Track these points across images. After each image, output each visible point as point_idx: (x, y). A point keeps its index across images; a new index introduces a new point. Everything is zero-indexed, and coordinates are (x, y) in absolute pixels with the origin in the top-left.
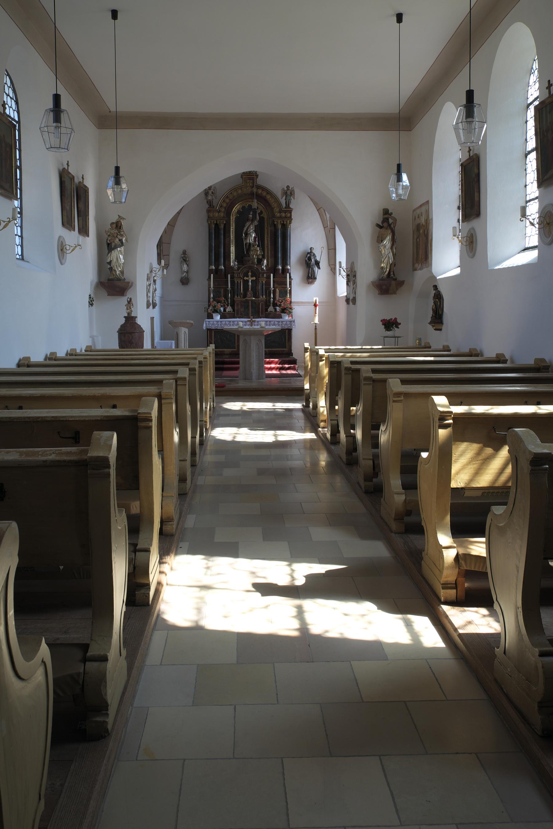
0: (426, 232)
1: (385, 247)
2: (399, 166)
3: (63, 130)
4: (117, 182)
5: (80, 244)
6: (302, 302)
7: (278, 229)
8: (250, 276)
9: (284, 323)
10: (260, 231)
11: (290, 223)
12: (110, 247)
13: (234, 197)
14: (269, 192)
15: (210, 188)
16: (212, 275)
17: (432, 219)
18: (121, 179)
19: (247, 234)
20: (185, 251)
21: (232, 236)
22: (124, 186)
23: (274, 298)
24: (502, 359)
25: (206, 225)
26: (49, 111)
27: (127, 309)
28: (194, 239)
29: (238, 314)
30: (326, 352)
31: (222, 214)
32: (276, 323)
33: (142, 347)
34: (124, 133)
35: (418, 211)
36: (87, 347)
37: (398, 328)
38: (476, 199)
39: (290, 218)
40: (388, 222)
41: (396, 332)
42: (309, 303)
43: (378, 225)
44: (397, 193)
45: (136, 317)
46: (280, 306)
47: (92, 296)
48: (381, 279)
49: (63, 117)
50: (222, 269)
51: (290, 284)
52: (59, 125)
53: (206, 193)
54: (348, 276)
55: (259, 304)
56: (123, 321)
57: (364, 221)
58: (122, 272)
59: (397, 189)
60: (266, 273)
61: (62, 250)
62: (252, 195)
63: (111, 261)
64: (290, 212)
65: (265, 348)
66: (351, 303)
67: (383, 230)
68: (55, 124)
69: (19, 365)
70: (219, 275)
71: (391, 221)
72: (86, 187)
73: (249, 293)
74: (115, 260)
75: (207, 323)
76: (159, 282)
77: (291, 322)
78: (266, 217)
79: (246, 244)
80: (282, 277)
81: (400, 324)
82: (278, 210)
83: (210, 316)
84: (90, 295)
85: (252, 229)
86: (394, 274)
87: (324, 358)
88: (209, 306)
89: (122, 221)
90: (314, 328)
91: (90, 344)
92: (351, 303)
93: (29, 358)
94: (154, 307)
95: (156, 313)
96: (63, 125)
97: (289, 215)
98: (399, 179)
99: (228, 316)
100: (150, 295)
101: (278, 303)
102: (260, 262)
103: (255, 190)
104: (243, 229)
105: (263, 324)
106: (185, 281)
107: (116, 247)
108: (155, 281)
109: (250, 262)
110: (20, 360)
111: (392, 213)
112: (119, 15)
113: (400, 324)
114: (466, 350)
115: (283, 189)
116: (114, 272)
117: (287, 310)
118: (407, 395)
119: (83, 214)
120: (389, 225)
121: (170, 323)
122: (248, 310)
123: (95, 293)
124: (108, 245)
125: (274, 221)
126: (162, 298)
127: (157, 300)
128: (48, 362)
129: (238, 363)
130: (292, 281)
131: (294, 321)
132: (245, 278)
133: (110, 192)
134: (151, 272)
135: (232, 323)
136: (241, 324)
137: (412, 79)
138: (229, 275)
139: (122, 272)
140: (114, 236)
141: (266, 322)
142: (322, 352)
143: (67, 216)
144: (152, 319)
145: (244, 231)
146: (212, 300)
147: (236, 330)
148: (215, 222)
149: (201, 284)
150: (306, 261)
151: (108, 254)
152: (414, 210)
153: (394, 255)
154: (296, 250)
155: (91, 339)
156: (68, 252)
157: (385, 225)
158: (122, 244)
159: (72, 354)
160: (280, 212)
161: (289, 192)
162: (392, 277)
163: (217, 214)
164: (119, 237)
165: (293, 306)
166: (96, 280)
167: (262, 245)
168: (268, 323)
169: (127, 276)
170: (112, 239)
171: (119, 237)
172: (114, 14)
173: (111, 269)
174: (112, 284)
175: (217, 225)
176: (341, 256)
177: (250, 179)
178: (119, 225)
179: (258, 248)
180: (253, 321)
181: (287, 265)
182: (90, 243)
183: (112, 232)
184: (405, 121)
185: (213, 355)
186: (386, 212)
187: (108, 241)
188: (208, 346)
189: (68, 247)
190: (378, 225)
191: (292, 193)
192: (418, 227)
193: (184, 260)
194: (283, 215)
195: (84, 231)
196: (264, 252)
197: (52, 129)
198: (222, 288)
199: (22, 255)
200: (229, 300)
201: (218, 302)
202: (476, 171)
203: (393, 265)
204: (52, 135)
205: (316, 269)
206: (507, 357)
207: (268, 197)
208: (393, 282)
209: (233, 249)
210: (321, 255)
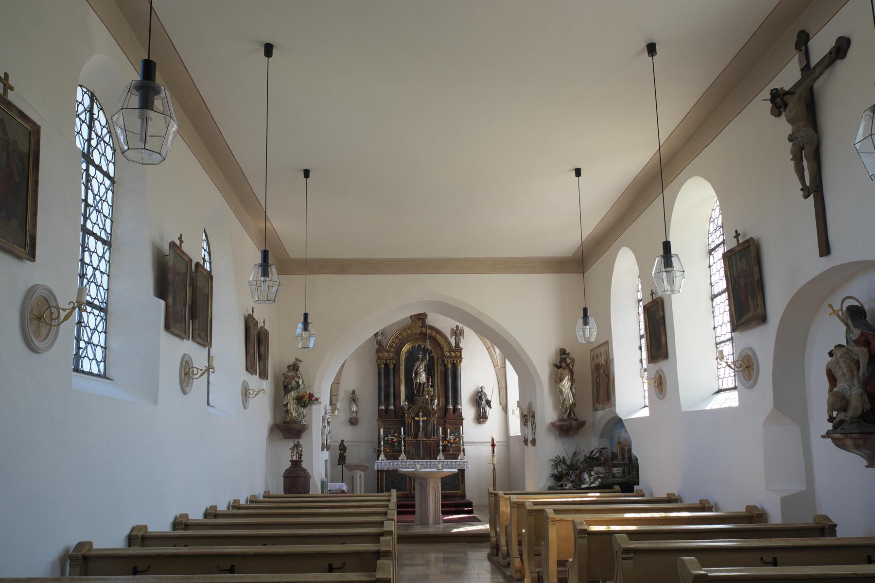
2: (585, 310)
10: (430, 371)
14: (438, 332)
17: (613, 359)
19: (416, 374)
21: (402, 377)
24: (707, 505)
35: (597, 351)
38: (663, 341)
39: (460, 358)
53: (376, 335)
56: (289, 465)
59: (584, 332)
65: (442, 490)
66: (529, 444)
68: (262, 278)
69: (206, 515)
71: (568, 361)
78: (435, 357)
85: (422, 369)
92: (529, 444)
100: (325, 437)
103: (424, 330)
105: (418, 466)
106: (353, 422)
110: (207, 510)
112: (311, 174)
114: (663, 495)
118: (637, 551)
119: (263, 357)
120: (568, 365)
124: (285, 387)
125: (443, 361)
128: (232, 511)
129: (414, 506)
132: (417, 418)
137: (590, 226)
145: (415, 368)
152: (592, 350)
154: (467, 390)
157: (564, 364)
159: (253, 500)
161: (458, 332)
172: (307, 173)
173: (287, 411)
174: (288, 428)
175: (386, 365)
177: (419, 319)
182: (266, 385)
184: (581, 264)
186: (563, 352)
189: (251, 392)
191: (462, 333)
195: (263, 375)
202: (661, 313)
205: (487, 408)
207: (438, 337)
208: (574, 423)
209: (403, 389)
210: (492, 394)
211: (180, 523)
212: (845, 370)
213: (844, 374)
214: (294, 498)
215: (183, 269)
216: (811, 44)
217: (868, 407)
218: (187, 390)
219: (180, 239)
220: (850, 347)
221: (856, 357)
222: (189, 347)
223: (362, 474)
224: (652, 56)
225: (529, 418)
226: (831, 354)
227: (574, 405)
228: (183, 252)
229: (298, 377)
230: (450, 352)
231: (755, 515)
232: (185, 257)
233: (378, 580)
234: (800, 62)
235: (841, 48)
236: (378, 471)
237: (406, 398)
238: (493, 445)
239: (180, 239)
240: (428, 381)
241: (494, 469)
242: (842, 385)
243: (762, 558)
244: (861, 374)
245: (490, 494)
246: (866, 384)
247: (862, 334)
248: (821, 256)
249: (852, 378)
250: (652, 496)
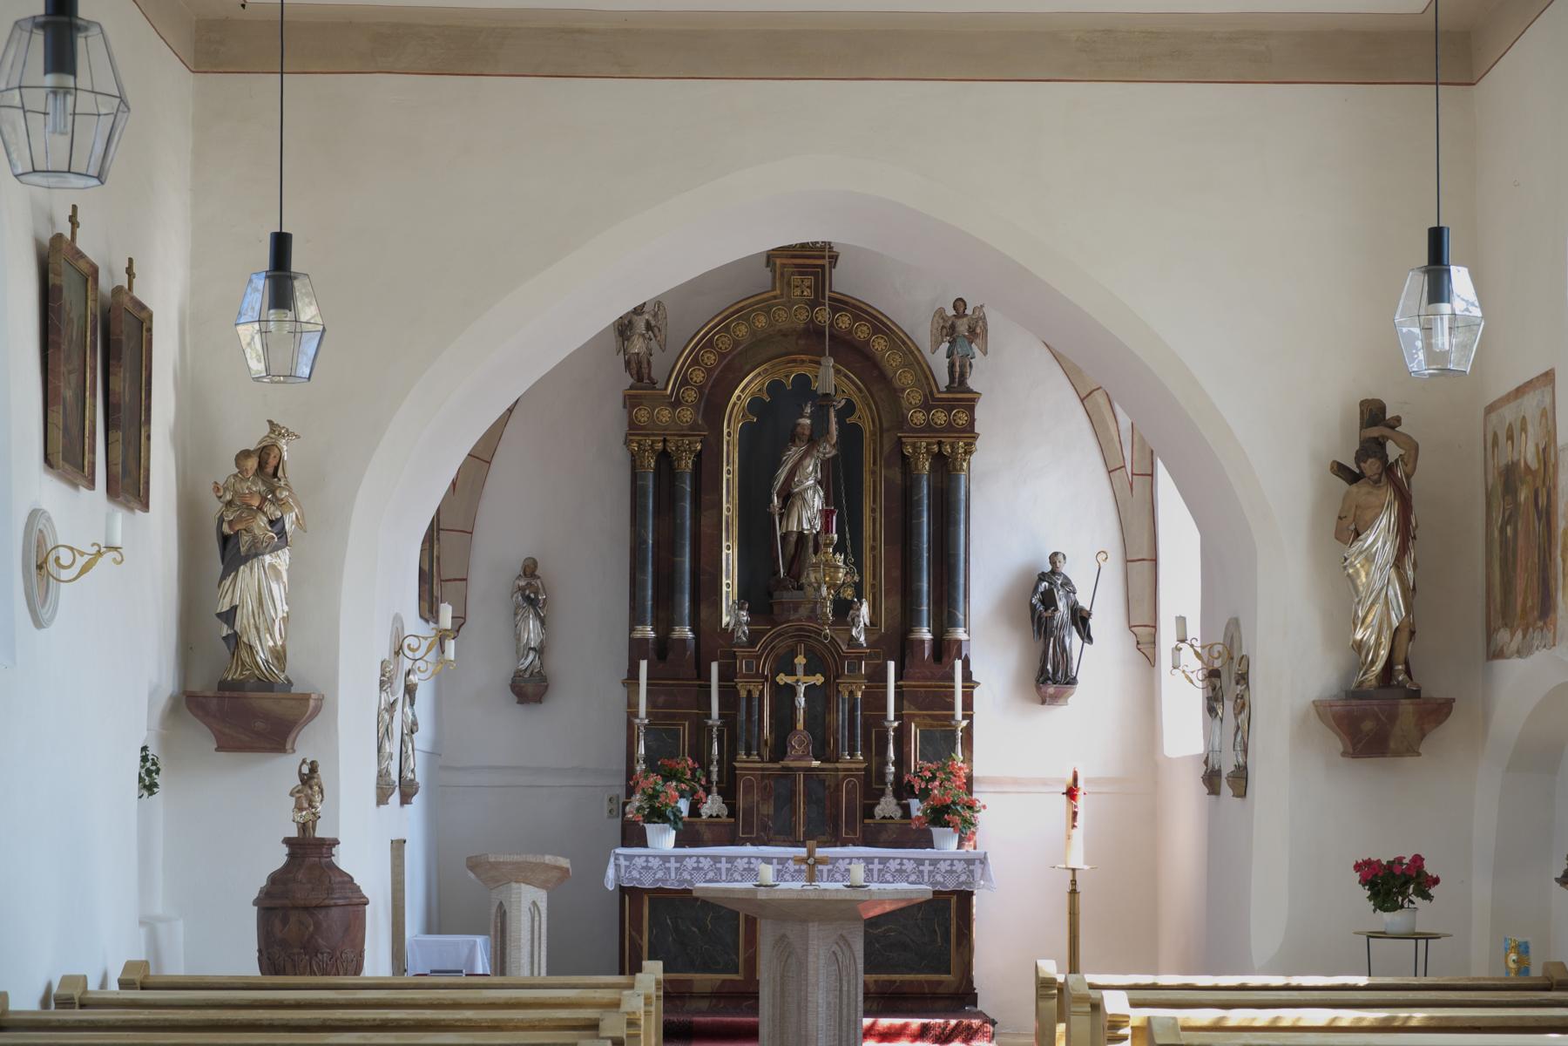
0: (1542, 501)
1: (1370, 559)
2: (1437, 238)
3: (85, 102)
4: (281, 294)
5: (118, 542)
6: (1016, 781)
7: (919, 477)
8: (800, 670)
9: (944, 866)
11: (968, 452)
12: (235, 552)
13: (736, 344)
14: (880, 325)
15: (638, 311)
16: (644, 665)
18: (296, 283)
19: (788, 497)
20: (535, 563)
21: (729, 506)
22: (307, 310)
23: (901, 762)
25: (621, 456)
26: (29, 26)
27: (300, 808)
28: (574, 520)
29: (748, 826)
30: (1135, 1004)
31: (687, 415)
32: (909, 866)
33: (358, 969)
34: (308, 91)
35: (1509, 414)
36: (129, 966)
37: (1428, 897)
39: (969, 432)
40: (1384, 457)
41: (1420, 914)
42: (1044, 782)
43: (1340, 470)
44: (1428, 346)
45: (335, 842)
46: (924, 795)
47: (151, 752)
48: (1355, 694)
49: (87, 49)
50: (684, 641)
51: (968, 704)
52: (69, 81)
53: (624, 328)
54: (1212, 675)
55: (838, 787)
56: (279, 857)
57: (1279, 453)
58: (280, 656)
59: (1428, 330)
60: (869, 657)
61: (40, 567)
62: (813, 338)
63: (234, 609)
64: (969, 404)
65: (866, 972)
66: (1226, 789)
68: (50, 80)
70: (672, 666)
71: (1393, 451)
72: (143, 307)
73: (799, 741)
74: (250, 604)
75: (623, 862)
76: (424, 695)
77: (970, 862)
79: (785, 537)
80: (934, 672)
81: (1436, 881)
82: (917, 399)
83: (633, 836)
84: (144, 749)
86: (1408, 672)
87: (1126, 1031)
88: (630, 792)
89: (282, 443)
90: (1068, 888)
91: (140, 955)
92: (1226, 789)
94: (405, 799)
95: (408, 821)
96: (83, 79)
97: (962, 419)
98: (1438, 291)
99: (707, 836)
100: (393, 747)
101: (918, 785)
102: (844, 610)
103: (824, 316)
104: (772, 476)
105: (858, 873)
106: (530, 688)
107: (255, 553)
108: (410, 690)
109: (804, 611)
111: (1398, 420)
113: (1436, 881)
115: (941, 311)
116: (244, 654)
117: (952, 812)
119: (129, 418)
120: (1389, 469)
121: (474, 865)
122: (794, 812)
123: (166, 741)
124: (225, 540)
125: (900, 443)
126: (433, 755)
127: (418, 769)
130: (976, 692)
131: (983, 861)
132: (782, 679)
133: (248, 332)
134: (398, 652)
135: (723, 865)
136: (768, 873)
138: (714, 667)
139: (280, 656)
140: (249, 507)
141: (868, 860)
142: (1115, 1003)
143: (66, 429)
144: (398, 846)
145: (782, 474)
146: (640, 767)
147: (749, 899)
148: (659, 446)
149: (599, 698)
150: (1033, 608)
151: (223, 577)
152: (1490, 409)
153: (1409, 592)
155: (143, 931)
156: (65, 575)
157: (1371, 466)
161: (962, 327)
162: (1401, 685)
163: (665, 415)
164: (268, 508)
165: (980, 795)
166: (167, 683)
167: (851, 546)
168: (876, 866)
169: (301, 671)
170: (239, 519)
171: (268, 508)
173: (234, 641)
174: (236, 704)
175: (664, 458)
176: (1181, 592)
177: (802, 270)
178: (272, 462)
179: (840, 558)
180: (819, 861)
181: (953, 623)
182: (154, 534)
183: (244, 488)
185: (657, 1007)
186: (1373, 414)
187: (226, 528)
188: (636, 968)
189: (65, 560)
190: (1340, 470)
191: (977, 331)
192: (1510, 477)
193: (527, 599)
194: (940, 418)
195: (129, 486)
196: (860, 573)
197: (36, 99)
198: (685, 717)
200: (714, 769)
201: (667, 778)
203: (1405, 635)
204: (36, 121)
205: (1074, 641)
207: (879, 344)
208: (1407, 707)
209: (730, 556)
210: (1095, 584)
214: (296, 990)
225: (1227, 681)
230: (927, 406)
236: (623, 890)
237: (745, 594)
238: (1071, 793)
240: (826, 527)
245: (1045, 986)
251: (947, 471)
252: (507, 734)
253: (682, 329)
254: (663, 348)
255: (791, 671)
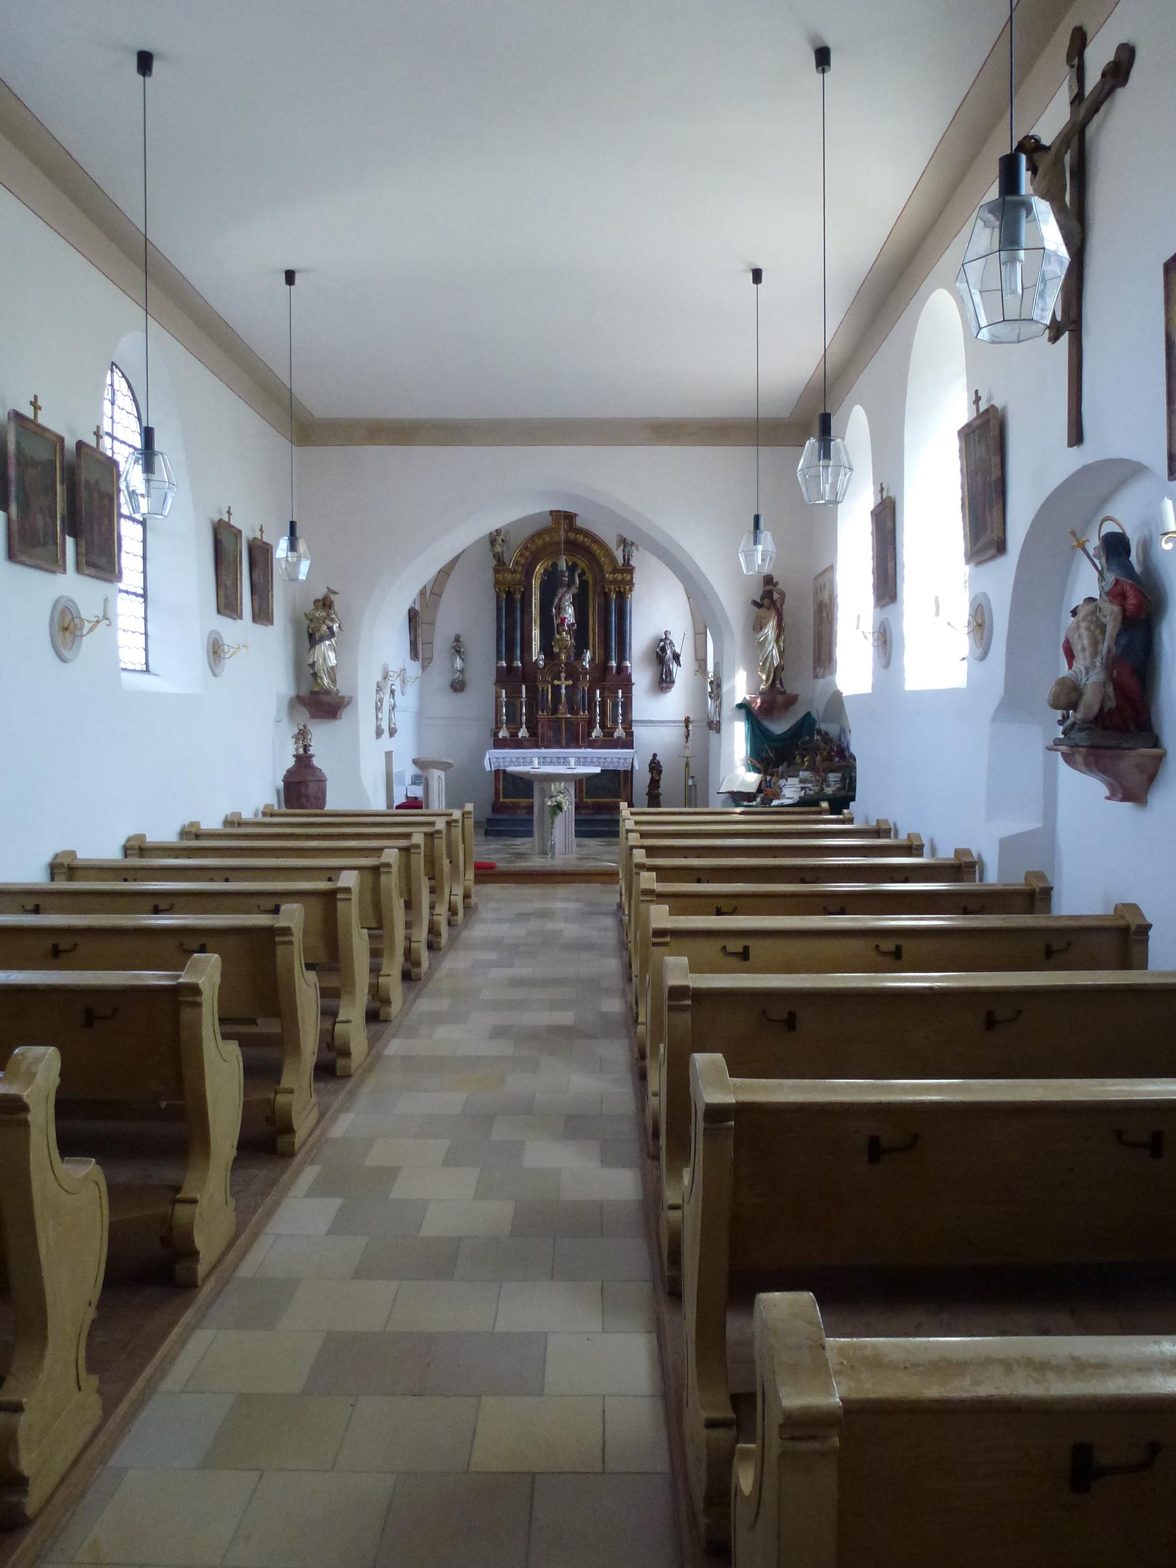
2: (757, 518)
6: (651, 722)
11: (631, 590)
12: (314, 639)
14: (595, 540)
15: (498, 532)
24: (916, 843)
25: (493, 593)
28: (470, 615)
33: (322, 805)
38: (891, 571)
39: (631, 583)
43: (755, 603)
53: (494, 539)
63: (314, 662)
67: (763, 612)
69: (126, 850)
70: (512, 677)
71: (776, 596)
73: (562, 708)
78: (591, 582)
82: (610, 569)
86: (781, 684)
93: (144, 836)
97: (628, 577)
100: (384, 715)
103: (572, 535)
104: (553, 599)
106: (458, 686)
107: (322, 639)
108: (392, 692)
118: (677, 934)
120: (773, 603)
124: (311, 636)
125: (603, 587)
132: (556, 682)
134: (385, 677)
144: (389, 755)
145: (556, 600)
152: (816, 578)
153: (782, 654)
154: (640, 638)
158: (332, 634)
160: (614, 572)
163: (509, 577)
169: (342, 688)
175: (509, 593)
181: (625, 659)
190: (755, 603)
194: (619, 577)
195: (263, 615)
199: (147, 663)
206: (925, 841)
207: (595, 547)
208: (780, 698)
209: (536, 633)
210: (682, 643)
211: (136, 847)
212: (1086, 641)
213: (1083, 649)
215: (43, 455)
216: (1089, 52)
217: (1111, 704)
218: (67, 654)
219: (35, 404)
220: (1100, 604)
221: (1104, 620)
222: (70, 584)
223: (442, 774)
224: (824, 71)
226: (1074, 613)
227: (778, 670)
228: (39, 426)
229: (332, 620)
231: (962, 867)
232: (47, 435)
233: (180, 984)
234: (1070, 87)
235: (1119, 70)
239: (35, 404)
241: (687, 764)
242: (1080, 663)
243: (877, 946)
244: (1105, 650)
246: (1111, 664)
247: (1117, 582)
248: (1070, 445)
249: (1095, 653)
250: (867, 821)
251: (622, 598)
252: (445, 703)
253: (518, 539)
254: (508, 549)
255: (559, 679)
